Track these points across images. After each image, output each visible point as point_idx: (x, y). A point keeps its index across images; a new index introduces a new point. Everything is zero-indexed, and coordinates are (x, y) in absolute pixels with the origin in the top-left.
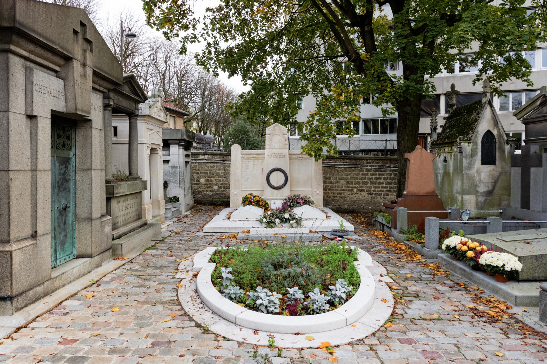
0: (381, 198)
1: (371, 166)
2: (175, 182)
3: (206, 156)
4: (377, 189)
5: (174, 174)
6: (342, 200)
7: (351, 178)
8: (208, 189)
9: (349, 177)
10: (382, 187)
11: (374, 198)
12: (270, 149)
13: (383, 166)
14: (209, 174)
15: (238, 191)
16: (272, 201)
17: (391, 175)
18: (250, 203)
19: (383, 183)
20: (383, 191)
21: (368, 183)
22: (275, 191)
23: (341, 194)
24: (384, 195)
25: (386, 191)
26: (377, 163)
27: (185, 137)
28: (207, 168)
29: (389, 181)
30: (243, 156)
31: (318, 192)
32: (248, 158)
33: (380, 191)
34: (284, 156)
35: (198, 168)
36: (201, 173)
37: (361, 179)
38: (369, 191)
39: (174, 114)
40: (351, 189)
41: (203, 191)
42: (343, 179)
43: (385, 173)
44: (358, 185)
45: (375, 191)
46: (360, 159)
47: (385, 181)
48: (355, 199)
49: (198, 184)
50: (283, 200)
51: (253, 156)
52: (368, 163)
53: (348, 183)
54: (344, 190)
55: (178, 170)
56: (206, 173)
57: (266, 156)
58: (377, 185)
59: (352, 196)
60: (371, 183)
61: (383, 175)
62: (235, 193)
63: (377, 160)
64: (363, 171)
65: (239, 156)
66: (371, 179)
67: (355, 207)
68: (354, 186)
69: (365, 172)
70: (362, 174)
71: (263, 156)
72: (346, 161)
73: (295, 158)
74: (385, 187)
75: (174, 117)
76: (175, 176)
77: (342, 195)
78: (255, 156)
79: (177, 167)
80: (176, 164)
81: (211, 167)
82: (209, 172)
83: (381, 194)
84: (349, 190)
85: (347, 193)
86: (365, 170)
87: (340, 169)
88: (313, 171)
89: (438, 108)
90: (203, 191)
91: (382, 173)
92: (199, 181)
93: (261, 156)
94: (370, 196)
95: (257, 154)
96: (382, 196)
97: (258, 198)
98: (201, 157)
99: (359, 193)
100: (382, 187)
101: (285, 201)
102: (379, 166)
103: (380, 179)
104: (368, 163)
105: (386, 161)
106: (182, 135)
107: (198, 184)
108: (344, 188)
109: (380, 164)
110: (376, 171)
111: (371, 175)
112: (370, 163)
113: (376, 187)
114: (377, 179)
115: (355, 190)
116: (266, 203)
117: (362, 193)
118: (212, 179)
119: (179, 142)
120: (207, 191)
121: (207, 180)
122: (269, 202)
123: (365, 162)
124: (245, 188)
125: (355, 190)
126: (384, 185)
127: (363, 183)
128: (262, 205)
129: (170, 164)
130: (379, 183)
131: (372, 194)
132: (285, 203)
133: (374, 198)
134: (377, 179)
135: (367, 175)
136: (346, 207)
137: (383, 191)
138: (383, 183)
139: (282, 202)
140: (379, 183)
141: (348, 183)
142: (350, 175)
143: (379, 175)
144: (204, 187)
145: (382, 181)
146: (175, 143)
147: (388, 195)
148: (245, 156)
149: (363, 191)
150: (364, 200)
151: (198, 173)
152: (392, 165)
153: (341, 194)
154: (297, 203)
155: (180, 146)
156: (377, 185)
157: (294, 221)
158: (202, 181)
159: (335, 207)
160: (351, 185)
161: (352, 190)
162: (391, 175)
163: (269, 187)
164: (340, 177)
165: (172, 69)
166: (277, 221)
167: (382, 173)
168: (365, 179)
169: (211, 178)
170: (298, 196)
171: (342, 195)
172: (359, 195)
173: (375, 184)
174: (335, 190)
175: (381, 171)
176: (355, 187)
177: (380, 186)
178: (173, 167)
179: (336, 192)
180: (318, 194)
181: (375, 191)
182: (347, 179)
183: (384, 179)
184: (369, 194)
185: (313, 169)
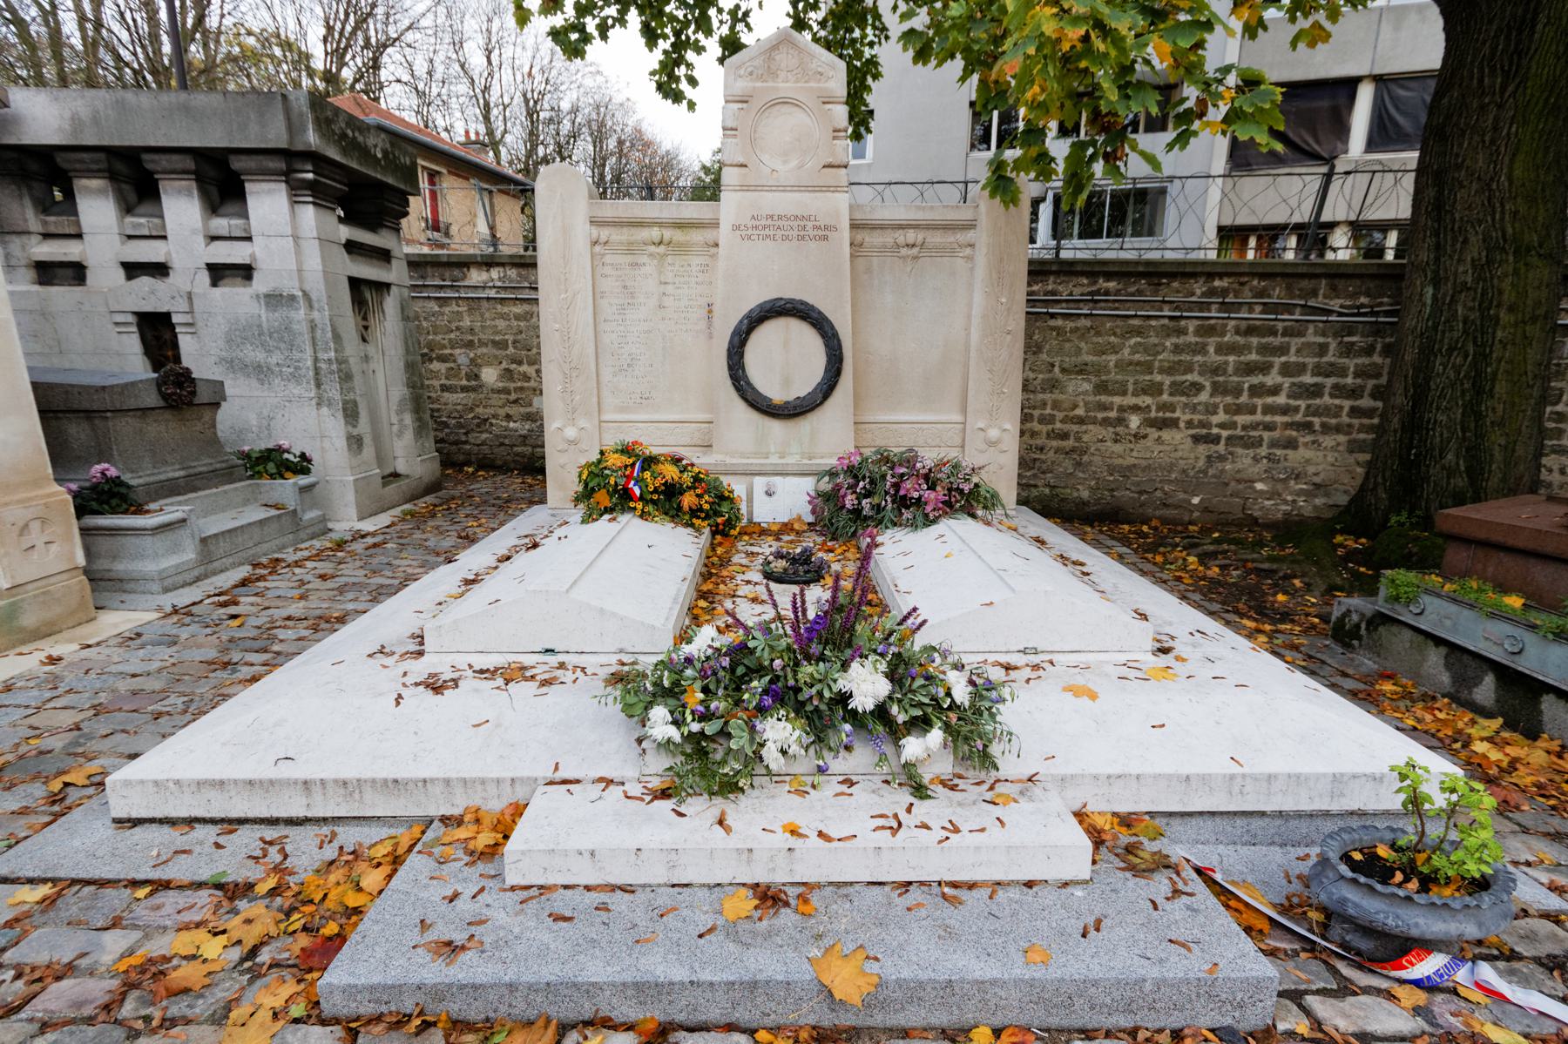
0: (1256, 459)
1: (1224, 306)
2: (295, 377)
3: (495, 273)
4: (1241, 419)
5: (285, 336)
6: (1068, 465)
7: (1121, 366)
8: (514, 410)
9: (1112, 359)
10: (1268, 410)
11: (1222, 458)
12: (745, 188)
13: (1289, 309)
14: (511, 350)
15: (582, 423)
16: (760, 483)
17: (1323, 349)
18: (622, 500)
19: (1275, 391)
20: (1269, 427)
21: (1198, 388)
22: (776, 427)
23: (1064, 436)
24: (1274, 444)
25: (1287, 426)
26: (1261, 293)
27: (312, 138)
28: (501, 324)
29: (1308, 379)
30: (605, 233)
31: (993, 433)
32: (631, 248)
33: (1254, 426)
34: (824, 233)
35: (466, 322)
36: (482, 344)
37: (1169, 371)
38: (1202, 425)
39: (487, 181)
40: (1113, 414)
41: (495, 416)
42: (1082, 370)
43: (1296, 342)
44: (1148, 400)
45: (1233, 425)
46: (1173, 276)
47: (1287, 382)
48: (1130, 461)
49: (474, 389)
50: (820, 475)
51: (655, 233)
52: (1212, 292)
53: (1102, 388)
54: (1081, 421)
55: (300, 314)
56: (502, 345)
57: (724, 233)
58: (1244, 399)
59: (1118, 448)
60: (1217, 389)
61: (1283, 350)
62: (571, 433)
63: (1263, 276)
64: (1182, 332)
65: (582, 232)
66: (1217, 370)
67: (1124, 495)
68: (1130, 400)
69: (1191, 338)
70: (1177, 349)
71: (709, 235)
72: (1103, 284)
73: (883, 249)
74: (1285, 410)
75: (490, 192)
76: (291, 347)
77: (1070, 443)
78: (668, 234)
79: (293, 298)
80: (291, 286)
81: (518, 317)
82: (510, 338)
83: (1259, 443)
84: (1106, 422)
85: (1093, 432)
86: (1192, 326)
87: (1070, 325)
88: (976, 321)
89: (1342, 129)
90: (495, 416)
91: (1277, 341)
92: (477, 377)
93: (697, 236)
94: (1202, 449)
95: (680, 225)
96: (1263, 451)
97: (671, 472)
98: (476, 276)
99: (1154, 433)
100: (1268, 410)
101: (826, 485)
102: (1267, 308)
103: (1265, 369)
104: (1212, 292)
105: (1305, 284)
106: (293, 128)
107: (474, 389)
108: (1080, 412)
109: (1277, 295)
110: (1250, 331)
111: (1220, 350)
112: (1224, 292)
113: (1239, 410)
114: (1250, 369)
115: (1134, 421)
116: (723, 497)
117: (1166, 435)
118: (524, 368)
119: (287, 163)
120: (508, 417)
121: (508, 374)
122: (738, 488)
123: (1199, 288)
124: (622, 410)
125: (1134, 421)
126: (1281, 399)
127: (1177, 389)
128: (695, 512)
129: (260, 284)
130: (1256, 391)
131: (1216, 440)
132: (826, 497)
133: (1222, 458)
134: (1250, 369)
135: (1201, 349)
136: (1085, 494)
137: (1269, 427)
138: (1275, 391)
139: (808, 485)
140: (1256, 391)
141: (1102, 388)
142: (1115, 350)
143: (1263, 350)
144: (497, 400)
145: (1272, 379)
146: (266, 174)
147: (1291, 444)
148: (618, 236)
149: (1172, 424)
150: (1171, 467)
151: (470, 345)
152: (1335, 304)
153: (1064, 436)
154: (903, 502)
155: (296, 189)
156: (1244, 399)
157: (936, 736)
158: (490, 375)
159: (1035, 492)
160: (1117, 400)
161: (1121, 421)
162: (1323, 349)
163: (740, 405)
164: (1069, 361)
165: (507, 74)
166: (780, 731)
167: (1277, 341)
168: (1189, 370)
169: (520, 363)
170: (910, 460)
171: (1070, 443)
172: (1149, 442)
173: (1237, 392)
174: (1042, 420)
175: (1274, 333)
176: (1136, 409)
177: (1259, 402)
178: (274, 299)
179: (1044, 429)
180: (992, 444)
181: (1233, 425)
182: (1100, 370)
183: (1286, 370)
184: (1197, 439)
185: (977, 311)
